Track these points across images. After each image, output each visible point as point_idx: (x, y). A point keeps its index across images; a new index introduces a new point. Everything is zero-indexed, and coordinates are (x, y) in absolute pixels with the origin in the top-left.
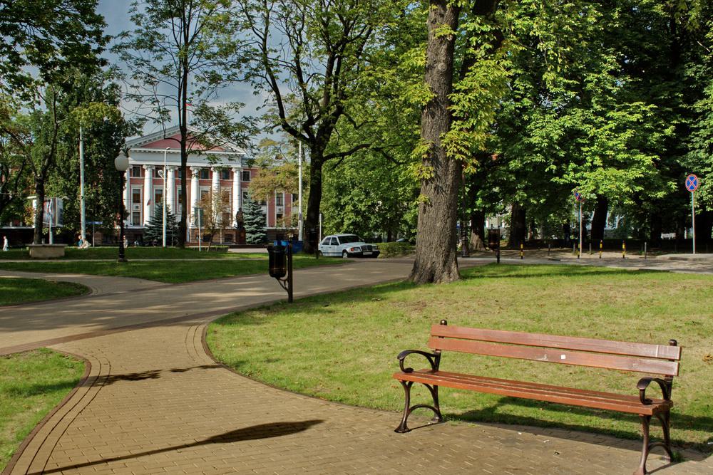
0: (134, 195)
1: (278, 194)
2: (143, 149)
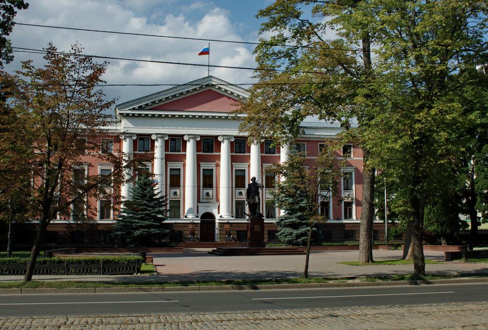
0: (237, 177)
1: (345, 174)
2: (150, 113)
